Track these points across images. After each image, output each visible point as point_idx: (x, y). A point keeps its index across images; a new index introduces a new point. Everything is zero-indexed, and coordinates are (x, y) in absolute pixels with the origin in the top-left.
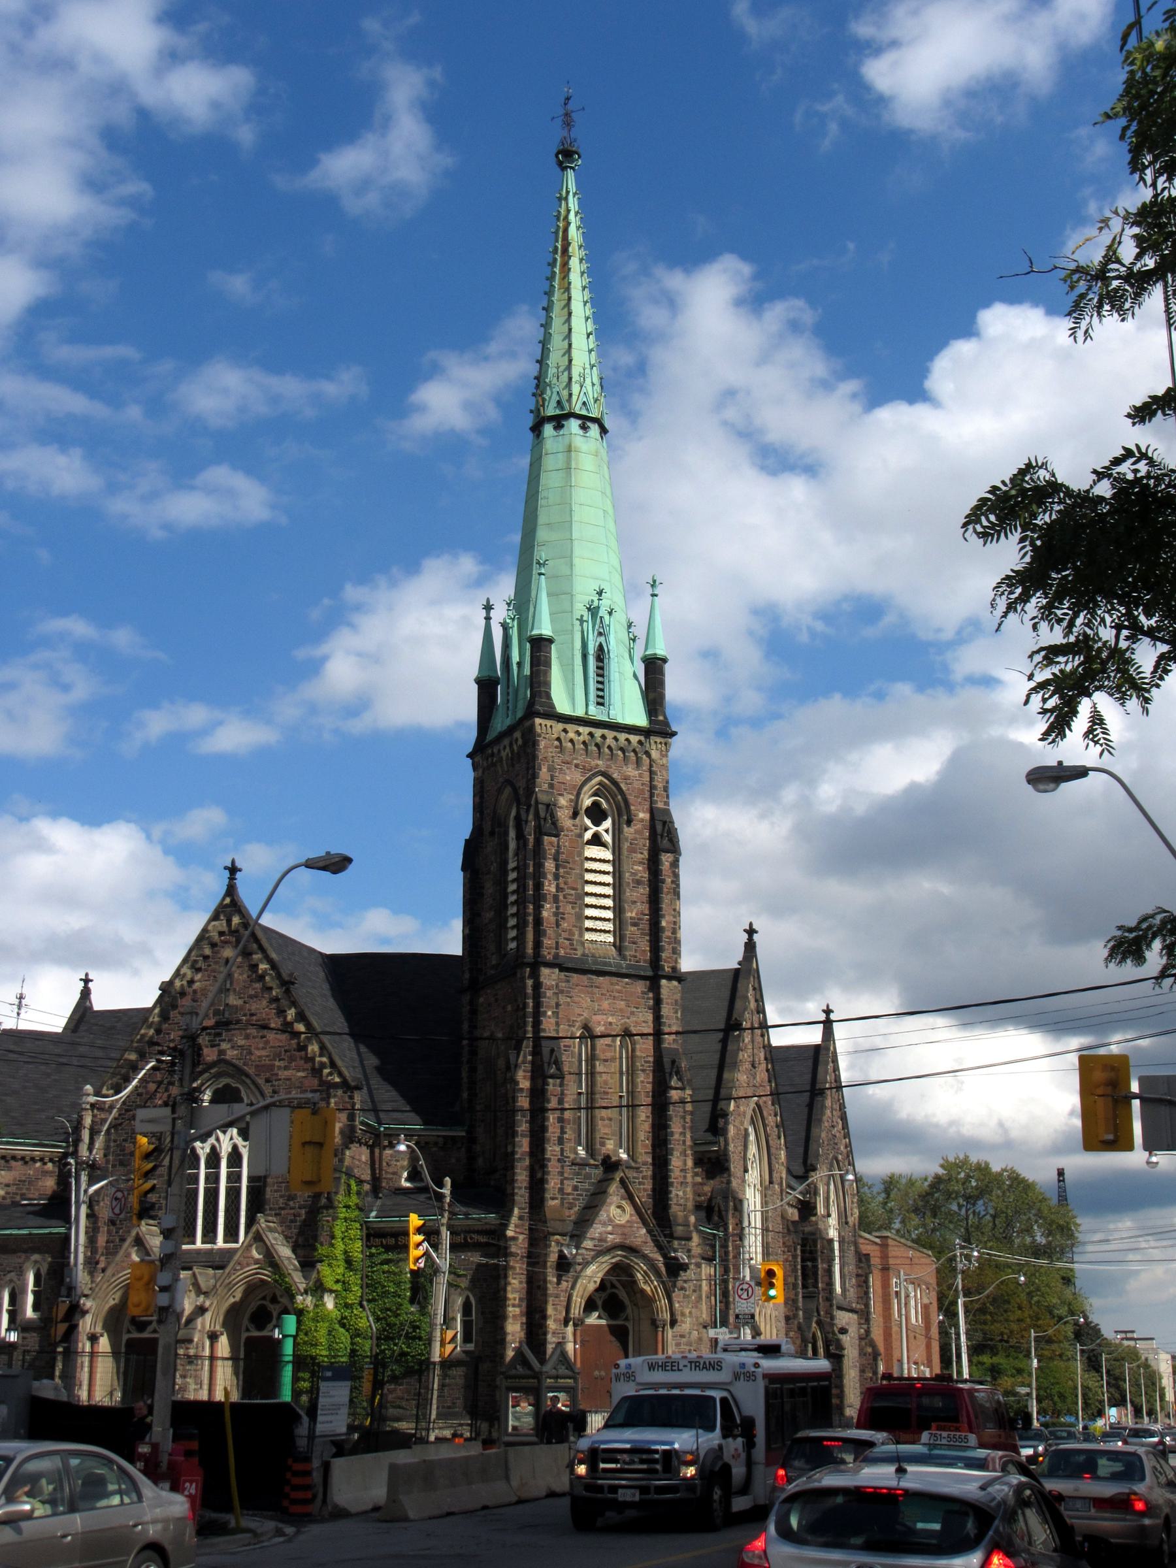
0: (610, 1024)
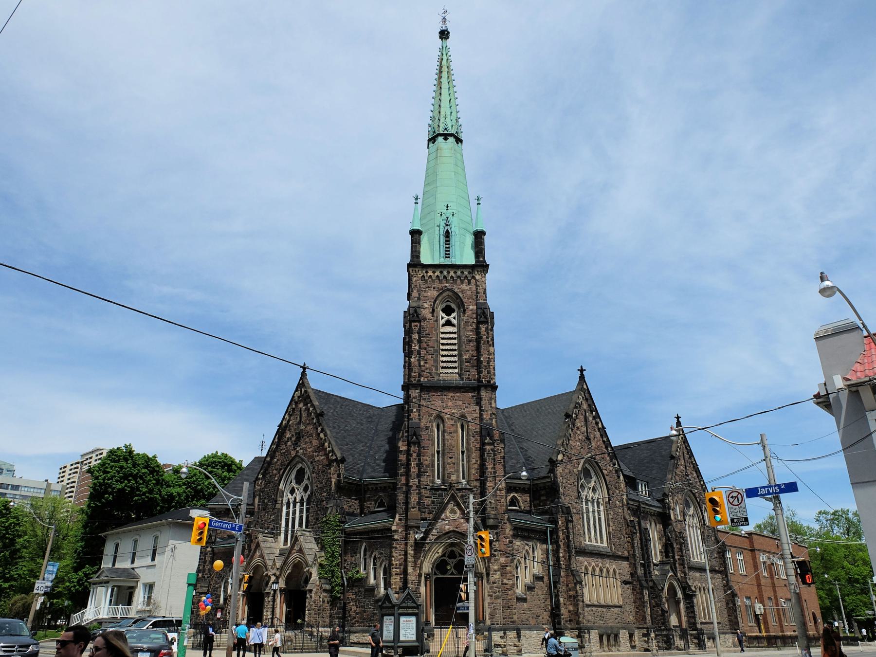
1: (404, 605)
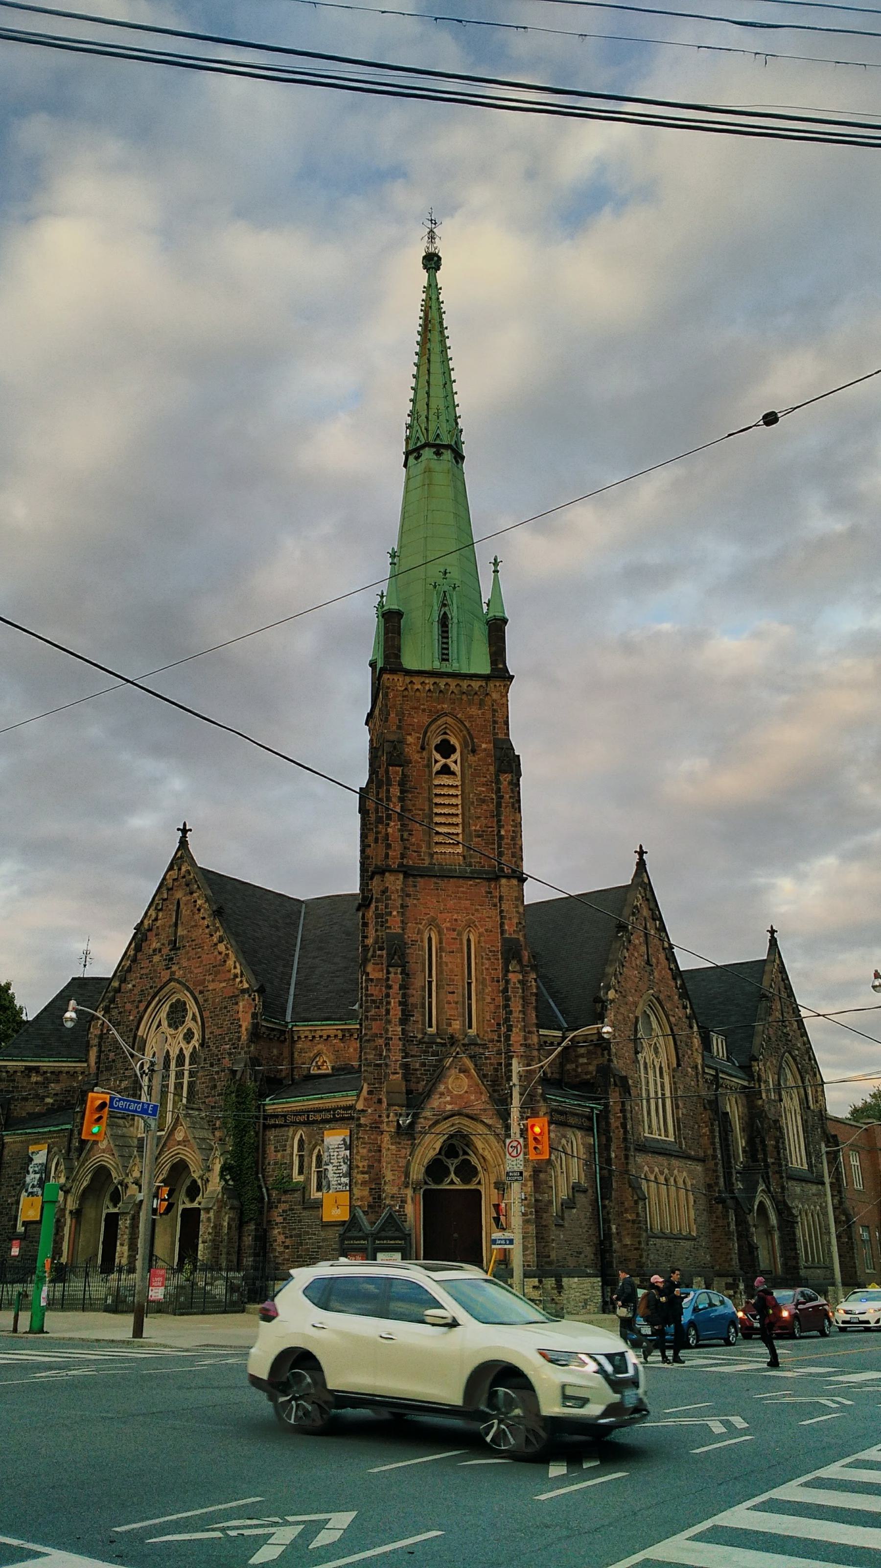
0: (456, 920)
1: (383, 1234)
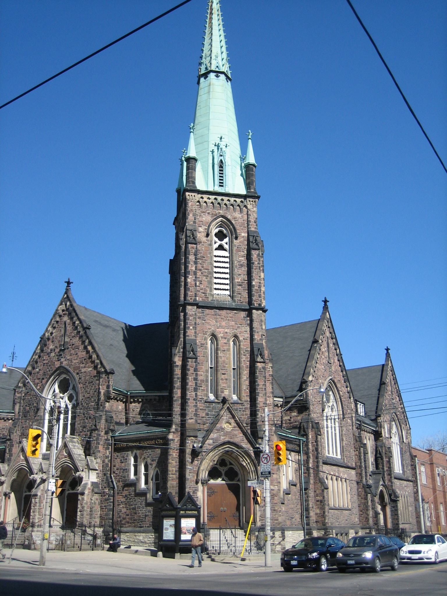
0: (226, 333)
